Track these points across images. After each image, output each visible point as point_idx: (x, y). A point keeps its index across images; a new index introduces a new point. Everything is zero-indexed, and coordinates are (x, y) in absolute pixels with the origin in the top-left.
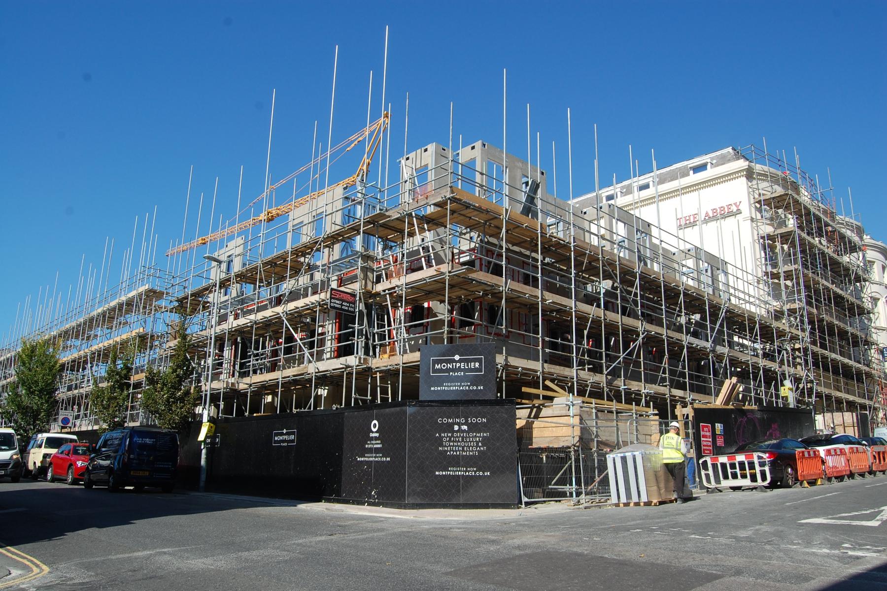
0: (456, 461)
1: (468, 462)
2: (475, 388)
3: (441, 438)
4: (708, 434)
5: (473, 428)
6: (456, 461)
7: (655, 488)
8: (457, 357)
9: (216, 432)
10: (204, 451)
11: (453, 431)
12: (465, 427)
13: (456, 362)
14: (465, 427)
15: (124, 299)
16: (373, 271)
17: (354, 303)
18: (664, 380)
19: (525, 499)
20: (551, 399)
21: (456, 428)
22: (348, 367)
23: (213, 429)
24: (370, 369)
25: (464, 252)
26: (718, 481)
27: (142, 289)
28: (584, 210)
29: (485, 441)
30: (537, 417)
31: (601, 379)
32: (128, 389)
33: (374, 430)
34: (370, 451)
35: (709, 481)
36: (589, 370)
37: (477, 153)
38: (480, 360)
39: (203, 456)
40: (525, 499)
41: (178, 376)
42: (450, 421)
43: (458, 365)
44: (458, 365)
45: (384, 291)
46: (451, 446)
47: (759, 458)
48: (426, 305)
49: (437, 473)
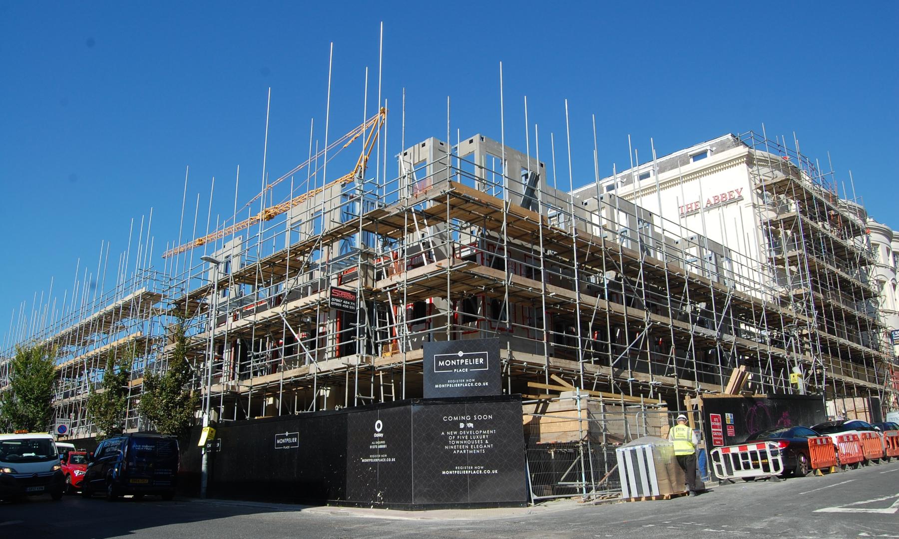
0: (462, 460)
1: (475, 460)
2: (480, 384)
3: (446, 436)
4: (718, 424)
5: (479, 425)
6: (462, 460)
7: (666, 481)
8: (461, 354)
9: (216, 436)
10: (205, 457)
11: (459, 429)
12: (471, 425)
13: (460, 358)
14: (471, 425)
15: (120, 302)
16: (373, 268)
17: (355, 301)
18: (671, 370)
19: (534, 497)
20: (557, 393)
21: (462, 425)
22: (350, 366)
23: (214, 434)
24: (372, 368)
25: (464, 247)
26: (730, 472)
27: (139, 292)
28: (585, 201)
29: (491, 438)
30: (544, 412)
31: (608, 371)
32: (126, 395)
33: (378, 430)
34: (375, 451)
35: (721, 472)
36: (595, 362)
37: (476, 147)
38: (484, 356)
39: (204, 461)
40: (534, 497)
41: (177, 380)
42: (456, 419)
43: (462, 361)
44: (462, 361)
45: (385, 288)
46: (457, 445)
47: (771, 447)
48: (428, 301)
49: (444, 473)
